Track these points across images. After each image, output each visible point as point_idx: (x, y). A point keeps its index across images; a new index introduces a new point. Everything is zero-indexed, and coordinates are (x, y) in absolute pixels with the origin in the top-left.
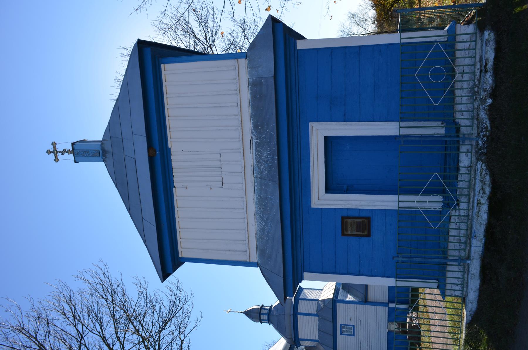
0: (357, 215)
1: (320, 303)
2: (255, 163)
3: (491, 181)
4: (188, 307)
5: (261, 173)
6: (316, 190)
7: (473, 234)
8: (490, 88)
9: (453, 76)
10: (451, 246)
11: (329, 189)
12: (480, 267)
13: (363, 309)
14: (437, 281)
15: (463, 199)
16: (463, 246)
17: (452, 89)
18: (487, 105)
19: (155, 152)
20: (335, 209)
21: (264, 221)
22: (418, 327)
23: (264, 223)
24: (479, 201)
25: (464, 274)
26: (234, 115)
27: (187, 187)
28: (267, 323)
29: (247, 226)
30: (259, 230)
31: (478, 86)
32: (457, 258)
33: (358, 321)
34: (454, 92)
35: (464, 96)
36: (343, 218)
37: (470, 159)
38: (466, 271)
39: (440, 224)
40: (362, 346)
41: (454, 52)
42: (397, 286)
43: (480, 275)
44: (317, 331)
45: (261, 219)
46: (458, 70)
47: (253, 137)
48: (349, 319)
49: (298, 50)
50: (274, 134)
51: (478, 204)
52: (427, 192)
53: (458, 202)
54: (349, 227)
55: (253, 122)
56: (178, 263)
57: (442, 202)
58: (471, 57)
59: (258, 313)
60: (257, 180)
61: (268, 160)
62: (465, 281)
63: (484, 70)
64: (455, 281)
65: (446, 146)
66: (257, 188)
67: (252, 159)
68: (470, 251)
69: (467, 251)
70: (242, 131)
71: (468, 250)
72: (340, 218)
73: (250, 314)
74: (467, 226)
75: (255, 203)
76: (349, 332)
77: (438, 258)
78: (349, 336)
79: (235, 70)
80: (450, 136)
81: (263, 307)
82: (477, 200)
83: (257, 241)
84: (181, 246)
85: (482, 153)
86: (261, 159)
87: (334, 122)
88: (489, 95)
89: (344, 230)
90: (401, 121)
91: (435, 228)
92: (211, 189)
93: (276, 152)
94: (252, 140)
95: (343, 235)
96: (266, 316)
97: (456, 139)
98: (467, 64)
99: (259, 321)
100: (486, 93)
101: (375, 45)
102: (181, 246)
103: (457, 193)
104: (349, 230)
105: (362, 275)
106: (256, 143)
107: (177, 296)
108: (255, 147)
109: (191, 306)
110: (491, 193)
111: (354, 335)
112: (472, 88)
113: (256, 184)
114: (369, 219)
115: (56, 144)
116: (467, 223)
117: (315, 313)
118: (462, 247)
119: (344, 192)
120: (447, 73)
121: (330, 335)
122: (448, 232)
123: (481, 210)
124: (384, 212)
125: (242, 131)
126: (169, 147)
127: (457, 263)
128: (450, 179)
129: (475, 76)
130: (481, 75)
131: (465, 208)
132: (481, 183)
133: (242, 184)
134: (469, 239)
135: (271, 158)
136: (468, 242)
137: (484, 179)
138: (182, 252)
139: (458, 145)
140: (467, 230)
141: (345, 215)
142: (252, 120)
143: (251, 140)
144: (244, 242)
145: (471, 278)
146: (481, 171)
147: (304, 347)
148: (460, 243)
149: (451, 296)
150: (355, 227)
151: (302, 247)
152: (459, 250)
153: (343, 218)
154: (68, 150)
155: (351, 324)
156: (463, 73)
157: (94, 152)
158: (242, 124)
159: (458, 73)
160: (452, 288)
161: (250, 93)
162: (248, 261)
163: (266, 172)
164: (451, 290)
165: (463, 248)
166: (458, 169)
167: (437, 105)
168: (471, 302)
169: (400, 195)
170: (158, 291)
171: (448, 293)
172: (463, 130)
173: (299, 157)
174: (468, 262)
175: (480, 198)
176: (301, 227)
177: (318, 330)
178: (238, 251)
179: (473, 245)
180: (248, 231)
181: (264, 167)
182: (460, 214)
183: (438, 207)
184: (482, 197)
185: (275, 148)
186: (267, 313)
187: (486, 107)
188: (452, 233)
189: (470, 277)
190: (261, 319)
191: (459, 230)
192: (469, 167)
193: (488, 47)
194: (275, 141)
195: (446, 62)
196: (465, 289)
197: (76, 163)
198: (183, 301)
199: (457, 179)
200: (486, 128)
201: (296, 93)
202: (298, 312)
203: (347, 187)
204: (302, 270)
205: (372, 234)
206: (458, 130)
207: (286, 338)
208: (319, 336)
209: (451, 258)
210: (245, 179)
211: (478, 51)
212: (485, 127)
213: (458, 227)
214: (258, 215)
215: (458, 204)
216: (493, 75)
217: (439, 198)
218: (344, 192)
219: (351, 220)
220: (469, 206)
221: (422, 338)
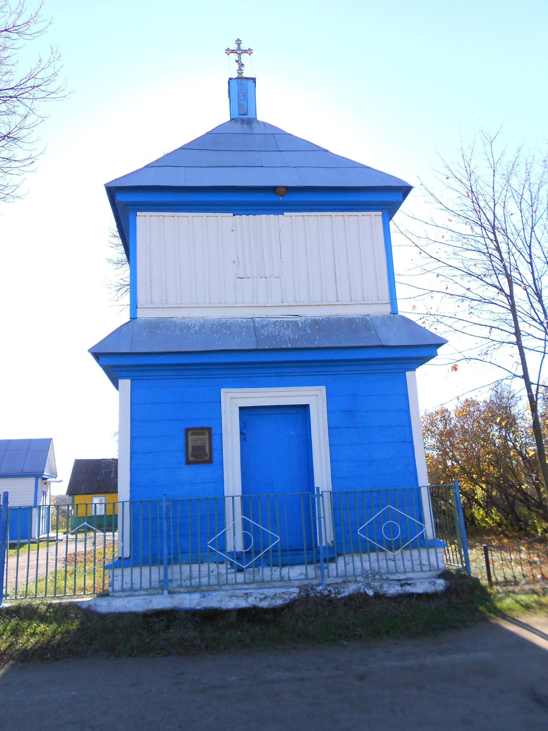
0: (215, 445)
3: (276, 606)
7: (207, 594)
8: (385, 591)
9: (390, 549)
10: (186, 568)
12: (161, 609)
17: (377, 549)
18: (366, 590)
19: (282, 195)
21: (200, 329)
23: (197, 328)
24: (251, 595)
26: (327, 297)
27: (234, 231)
31: (381, 579)
36: (209, 429)
39: (215, 550)
43: (150, 610)
45: (200, 325)
49: (405, 372)
50: (316, 344)
51: (247, 594)
54: (198, 437)
55: (321, 319)
58: (413, 568)
61: (282, 337)
63: (403, 583)
64: (127, 579)
68: (180, 592)
69: (178, 590)
72: (208, 426)
75: (219, 318)
82: (251, 593)
83: (167, 319)
84: (152, 216)
85: (308, 591)
88: (377, 591)
91: (210, 544)
94: (298, 317)
95: (187, 430)
97: (322, 560)
100: (379, 588)
102: (152, 216)
104: (194, 437)
105: (131, 457)
110: (262, 609)
112: (379, 573)
114: (210, 461)
115: (250, 55)
123: (239, 599)
124: (221, 480)
127: (162, 578)
128: (272, 557)
129: (392, 573)
130: (393, 580)
132: (273, 594)
134: (195, 590)
137: (278, 597)
140: (209, 585)
141: (213, 432)
142: (322, 318)
143: (298, 316)
145: (145, 599)
146: (288, 593)
150: (199, 445)
153: (209, 429)
154: (243, 70)
157: (246, 108)
161: (354, 316)
163: (266, 334)
167: (359, 533)
168: (109, 603)
169: (241, 497)
172: (332, 566)
174: (166, 592)
175: (255, 595)
176: (195, 377)
179: (192, 595)
181: (272, 332)
184: (256, 598)
187: (362, 590)
193: (428, 585)
194: (309, 346)
195: (405, 540)
197: (228, 79)
200: (339, 593)
204: (134, 378)
205: (190, 466)
206: (332, 560)
211: (422, 575)
212: (339, 591)
216: (398, 593)
217: (240, 548)
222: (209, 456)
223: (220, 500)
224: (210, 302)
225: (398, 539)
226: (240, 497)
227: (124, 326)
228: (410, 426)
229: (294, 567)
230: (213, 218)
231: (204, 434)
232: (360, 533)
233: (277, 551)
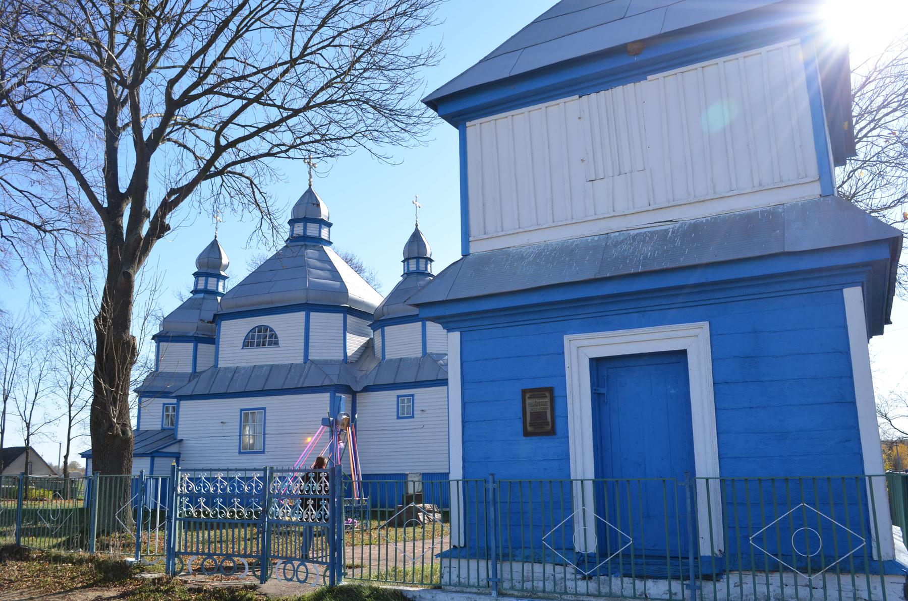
0: (558, 412)
1: (444, 358)
2: (632, 232)
4: (406, 139)
5: (615, 246)
6: (593, 342)
9: (804, 570)
10: (517, 566)
11: (597, 364)
13: (442, 432)
14: (462, 545)
15: (592, 586)
16: (518, 586)
17: (781, 568)
20: (565, 376)
22: (416, 524)
23: (531, 259)
25: (476, 587)
26: (714, 187)
28: (404, 271)
29: (526, 231)
30: (521, 251)
32: (499, 576)
33: (420, 423)
34: (776, 571)
35: (768, 588)
36: (551, 390)
37: (660, 598)
38: (481, 590)
40: (382, 432)
41: (849, 572)
42: (449, 482)
44: (399, 357)
46: (817, 578)
47: (678, 225)
48: (423, 409)
49: (841, 290)
50: (682, 262)
52: (601, 529)
53: (587, 578)
54: (538, 400)
56: (457, 120)
57: (586, 551)
59: (418, 254)
60: (603, 239)
61: (636, 256)
62: (465, 590)
64: (464, 573)
65: (678, 557)
66: (589, 240)
67: (638, 227)
69: (511, 592)
70: (687, 204)
71: (513, 594)
72: (549, 386)
73: (416, 239)
74: (548, 593)
76: (403, 410)
77: (497, 547)
78: (396, 410)
79: (798, 178)
80: (696, 566)
81: (429, 262)
86: (639, 244)
87: (713, 365)
89: (530, 394)
90: (721, 481)
92: (583, 160)
93: (648, 269)
95: (524, 392)
96: (415, 269)
97: (692, 574)
98: (828, 594)
99: (407, 257)
101: (858, 430)
103: (603, 575)
105: (463, 427)
106: (666, 231)
107: (421, 118)
108: (654, 231)
109: (409, 144)
111: (398, 418)
113: (596, 238)
114: (552, 432)
116: (555, 592)
117: (427, 352)
118: (517, 584)
119: (595, 390)
120: (809, 560)
121: (416, 378)
122: (540, 562)
124: (565, 458)
125: (687, 204)
126: (649, 77)
131: (578, 590)
133: (595, 214)
135: (640, 260)
136: (525, 594)
138: (474, 127)
139: (681, 577)
140: (544, 591)
143: (671, 221)
144: (499, 229)
147: (372, 337)
148: (523, 581)
149: (441, 568)
151: (498, 326)
152: (512, 579)
153: (551, 390)
155: (415, 413)
156: (811, 587)
158: (700, 202)
159: (810, 579)
160: (452, 569)
161: (757, 210)
162: (471, 239)
164: (450, 567)
165: (515, 585)
166: (642, 577)
167: (751, 542)
168: (433, 597)
170: (424, 84)
171: (446, 562)
172: (708, 587)
173: (647, 309)
174: (494, 593)
177: (401, 358)
178: (484, 221)
180: (517, 233)
181: (625, 250)
182: (570, 581)
183: (579, 547)
185: (656, 267)
186: (420, 269)
188: (538, 568)
189: (470, 596)
190: (410, 261)
191: (542, 579)
192: (646, 595)
194: (669, 265)
195: (830, 558)
196: (454, 589)
198: (415, 130)
199: (625, 575)
201: (761, 294)
202: (427, 322)
203: (604, 394)
205: (529, 438)
206: (707, 578)
207: (383, 306)
208: (391, 360)
209: (499, 566)
210: (604, 218)
213: (548, 578)
214: (545, 246)
215: (584, 578)
217: (592, 547)
218: (595, 390)
219: (549, 404)
220: (582, 595)
221: (402, 530)
222: (550, 426)
223: (566, 484)
224: (553, 219)
225: (819, 555)
226: (592, 481)
227: (453, 266)
228: (851, 376)
229: (658, 580)
230: (554, 107)
231: (544, 397)
232: (753, 542)
233: (629, 556)
